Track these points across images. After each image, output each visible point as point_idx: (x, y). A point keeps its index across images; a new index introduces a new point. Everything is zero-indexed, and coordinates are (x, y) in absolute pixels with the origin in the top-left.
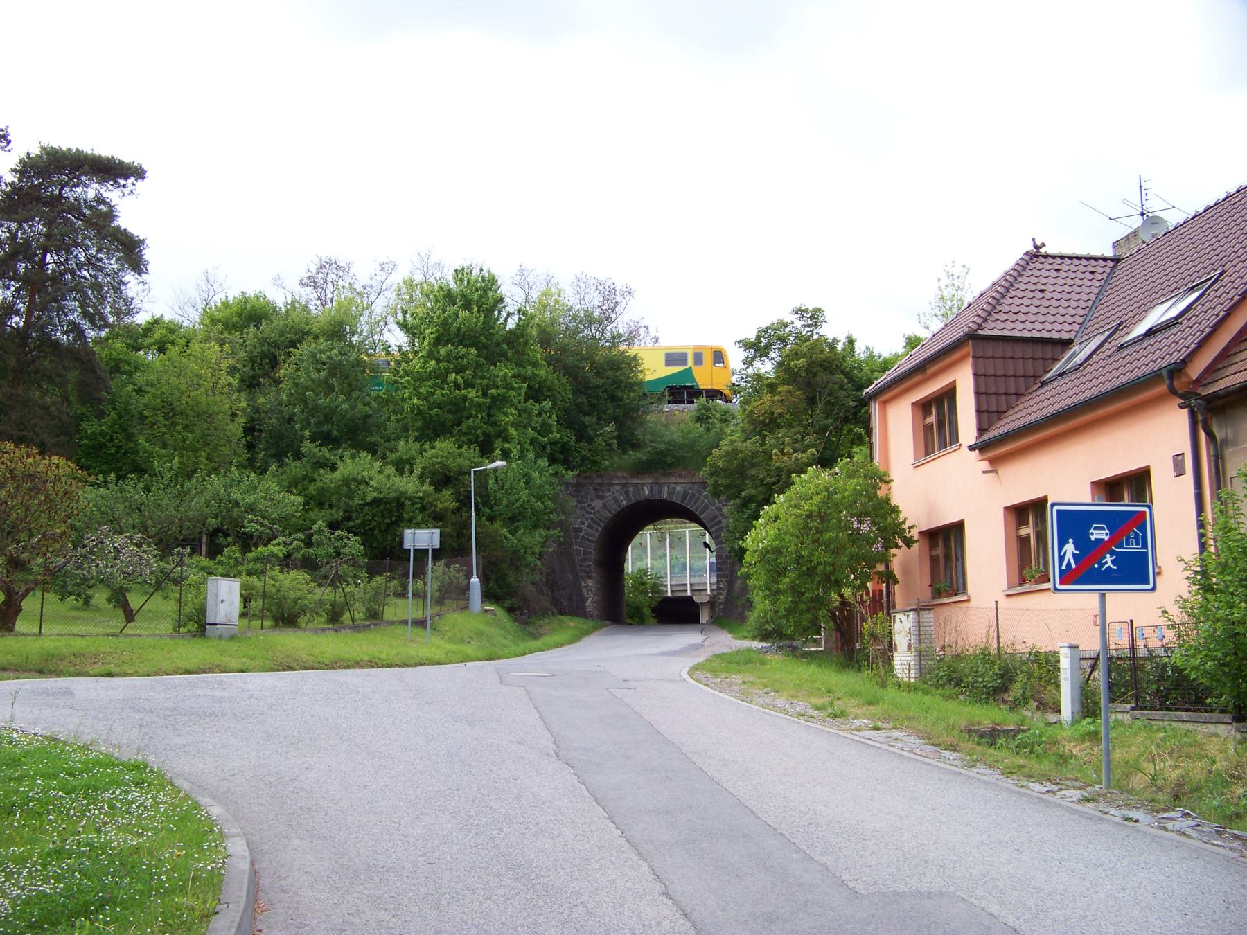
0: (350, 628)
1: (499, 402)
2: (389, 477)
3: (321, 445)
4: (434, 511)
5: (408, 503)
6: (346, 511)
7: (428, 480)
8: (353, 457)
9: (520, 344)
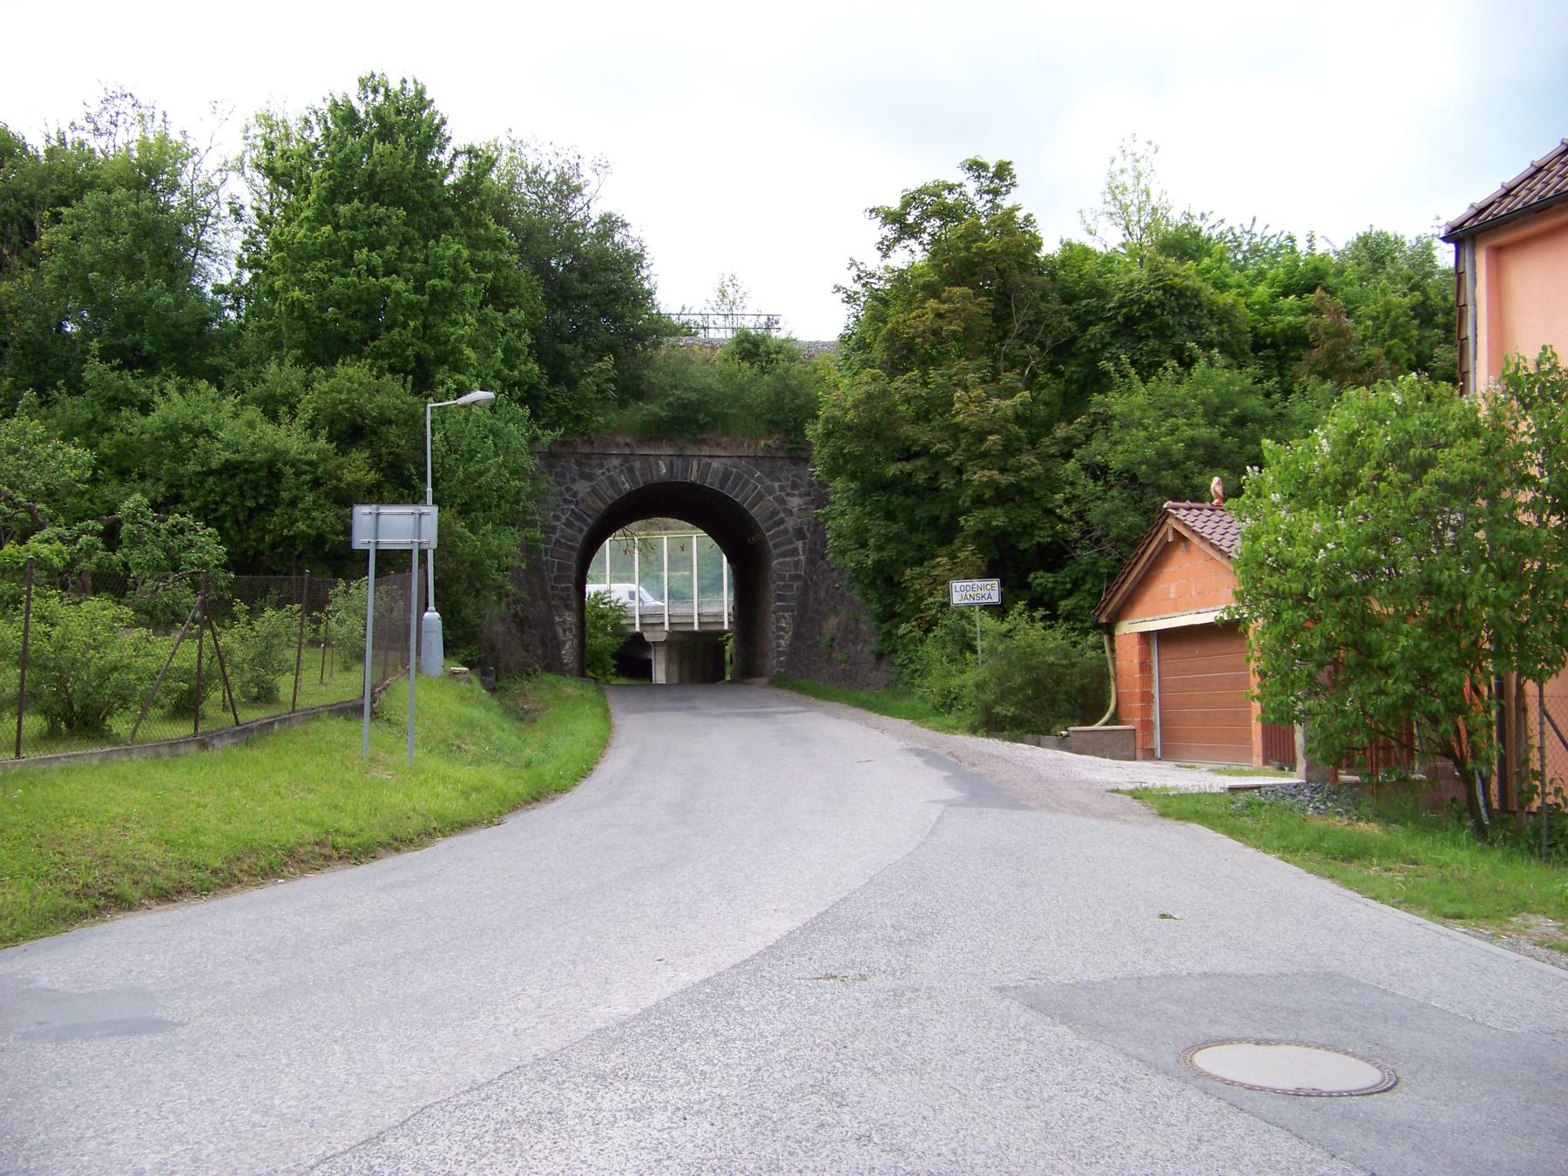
0: (233, 735)
1: (443, 302)
2: (251, 425)
3: (120, 368)
4: (336, 488)
5: (289, 471)
6: (171, 486)
7: (324, 432)
8: (182, 390)
9: (472, 207)
